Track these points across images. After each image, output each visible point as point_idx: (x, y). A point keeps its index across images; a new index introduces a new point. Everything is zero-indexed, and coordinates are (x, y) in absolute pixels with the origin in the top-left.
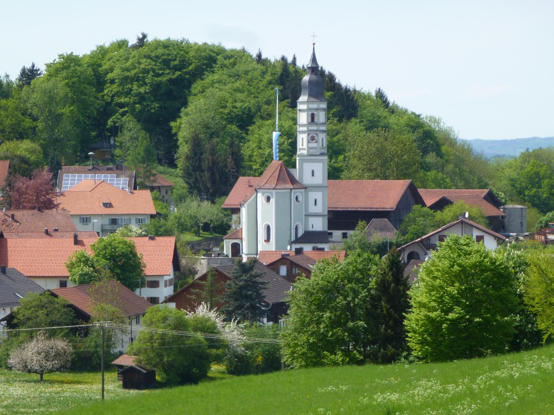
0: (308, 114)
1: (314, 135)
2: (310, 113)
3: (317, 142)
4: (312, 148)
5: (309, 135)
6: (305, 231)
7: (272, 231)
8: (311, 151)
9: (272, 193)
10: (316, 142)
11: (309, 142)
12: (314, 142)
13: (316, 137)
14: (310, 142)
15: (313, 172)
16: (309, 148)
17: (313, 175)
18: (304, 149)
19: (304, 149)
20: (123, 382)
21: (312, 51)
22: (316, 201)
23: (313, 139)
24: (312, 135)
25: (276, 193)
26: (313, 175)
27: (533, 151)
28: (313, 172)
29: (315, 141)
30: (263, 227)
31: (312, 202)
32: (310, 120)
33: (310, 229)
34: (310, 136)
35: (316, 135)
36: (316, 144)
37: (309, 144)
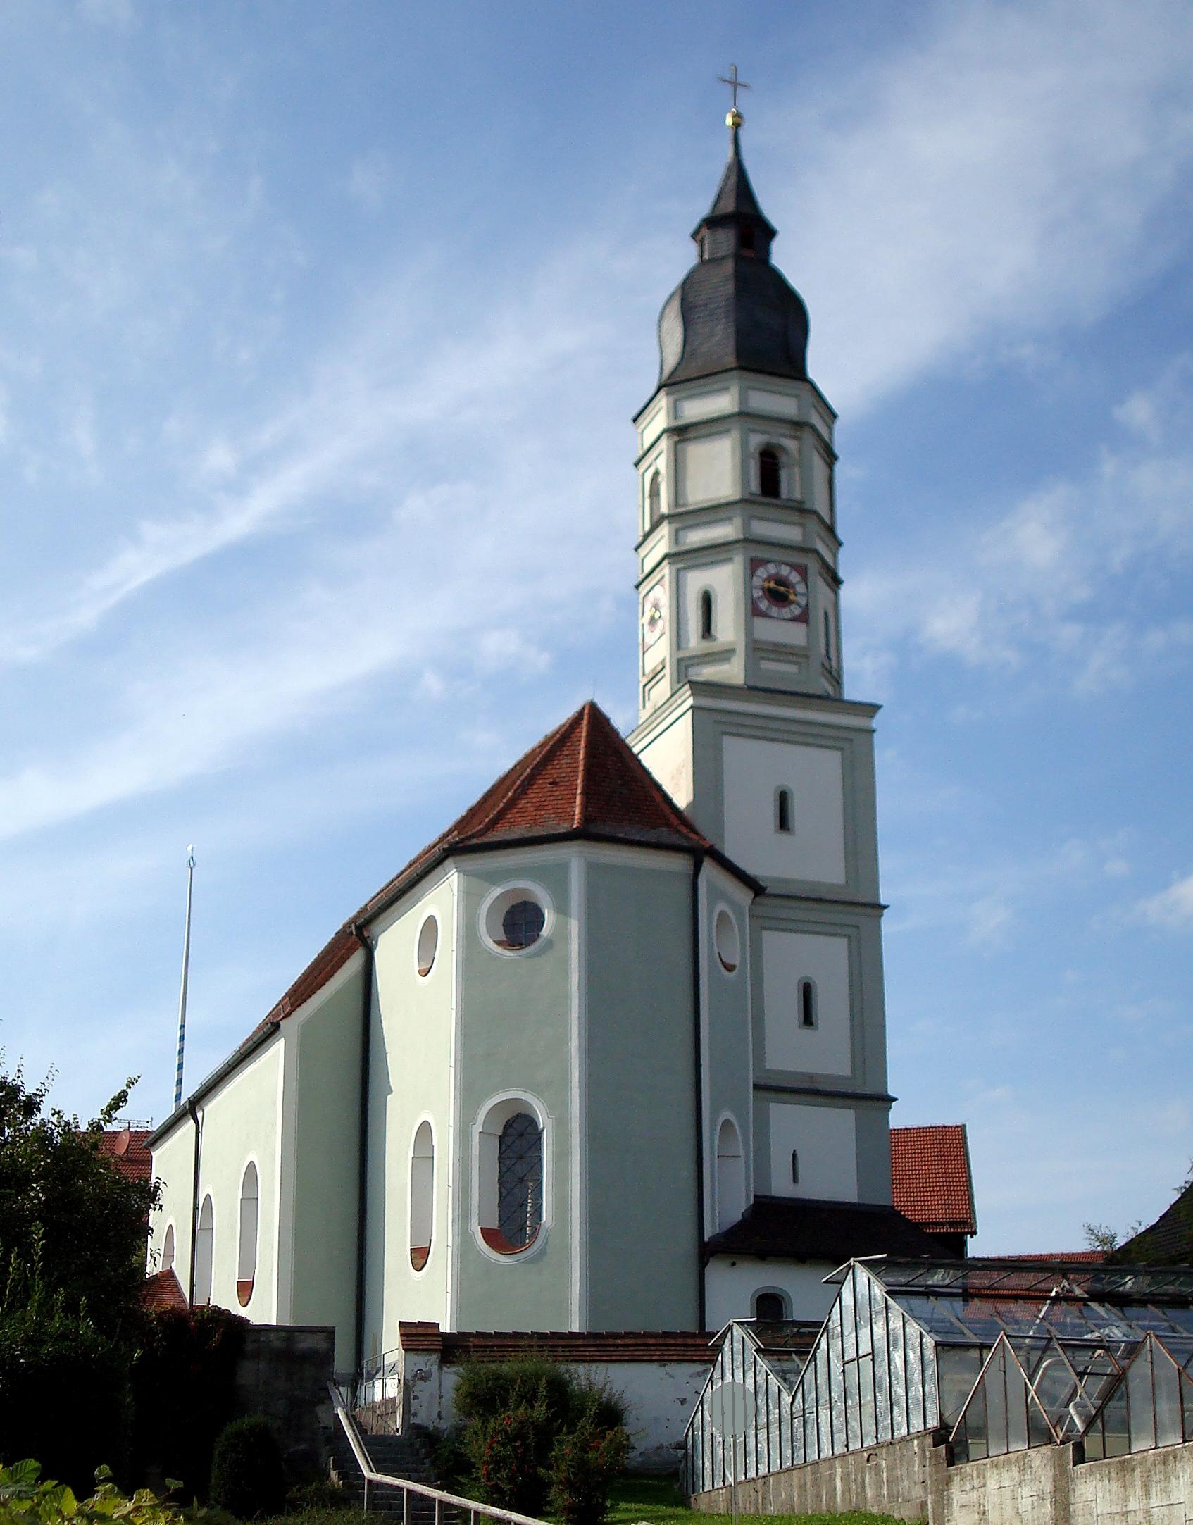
0: (744, 444)
1: (785, 571)
2: (757, 441)
3: (803, 618)
4: (780, 651)
5: (754, 565)
6: (755, 1196)
7: (561, 1156)
8: (767, 665)
9: (556, 880)
10: (795, 619)
11: (754, 611)
12: (786, 612)
13: (801, 588)
14: (764, 615)
15: (783, 800)
16: (757, 650)
17: (784, 823)
18: (724, 655)
19: (724, 655)
20: (632, 754)
21: (730, 154)
22: (807, 992)
23: (778, 594)
24: (772, 569)
25: (592, 869)
26: (784, 823)
27: (709, 1238)
28: (783, 800)
29: (797, 611)
30: (478, 1127)
31: (785, 1005)
32: (755, 486)
33: (781, 1187)
34: (762, 573)
35: (794, 578)
36: (801, 628)
37: (759, 622)
